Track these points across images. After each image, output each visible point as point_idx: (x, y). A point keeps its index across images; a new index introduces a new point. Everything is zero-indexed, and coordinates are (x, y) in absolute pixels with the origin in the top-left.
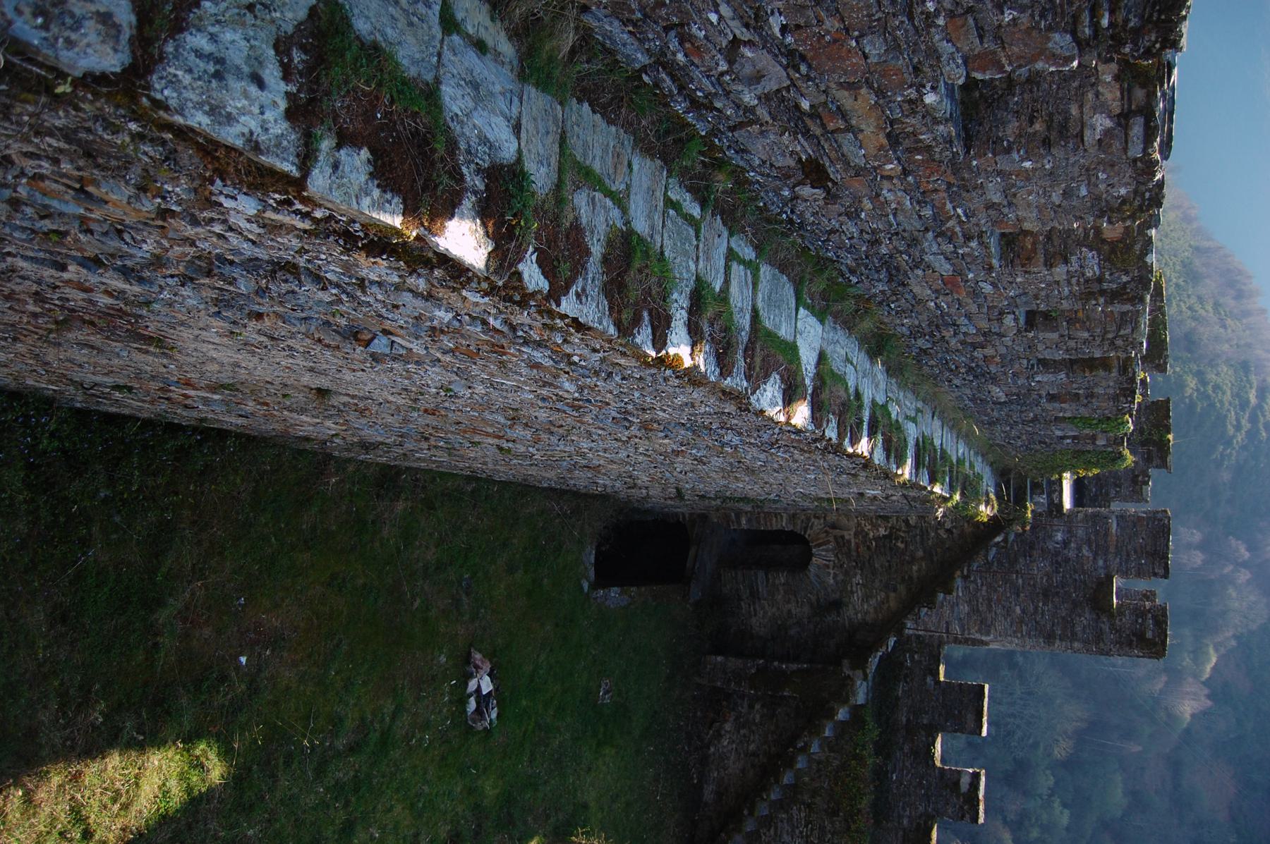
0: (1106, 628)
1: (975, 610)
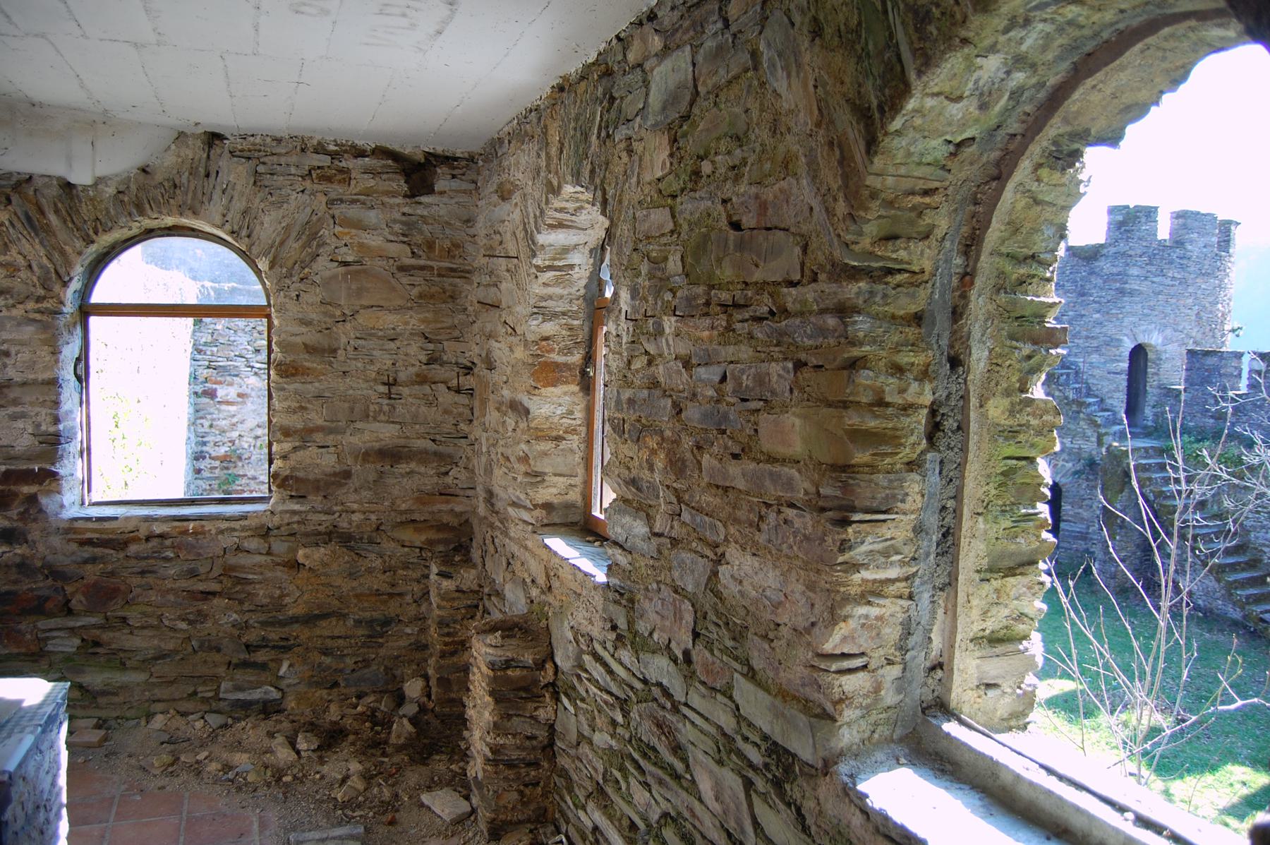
0: (1112, 250)
1: (1097, 349)
